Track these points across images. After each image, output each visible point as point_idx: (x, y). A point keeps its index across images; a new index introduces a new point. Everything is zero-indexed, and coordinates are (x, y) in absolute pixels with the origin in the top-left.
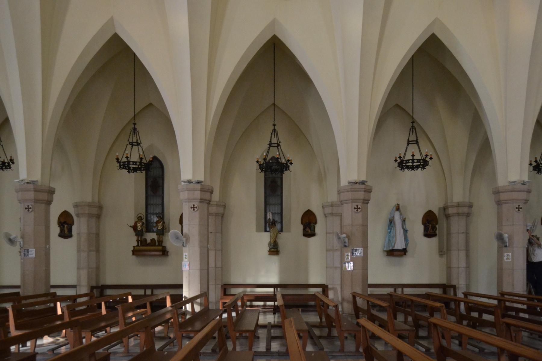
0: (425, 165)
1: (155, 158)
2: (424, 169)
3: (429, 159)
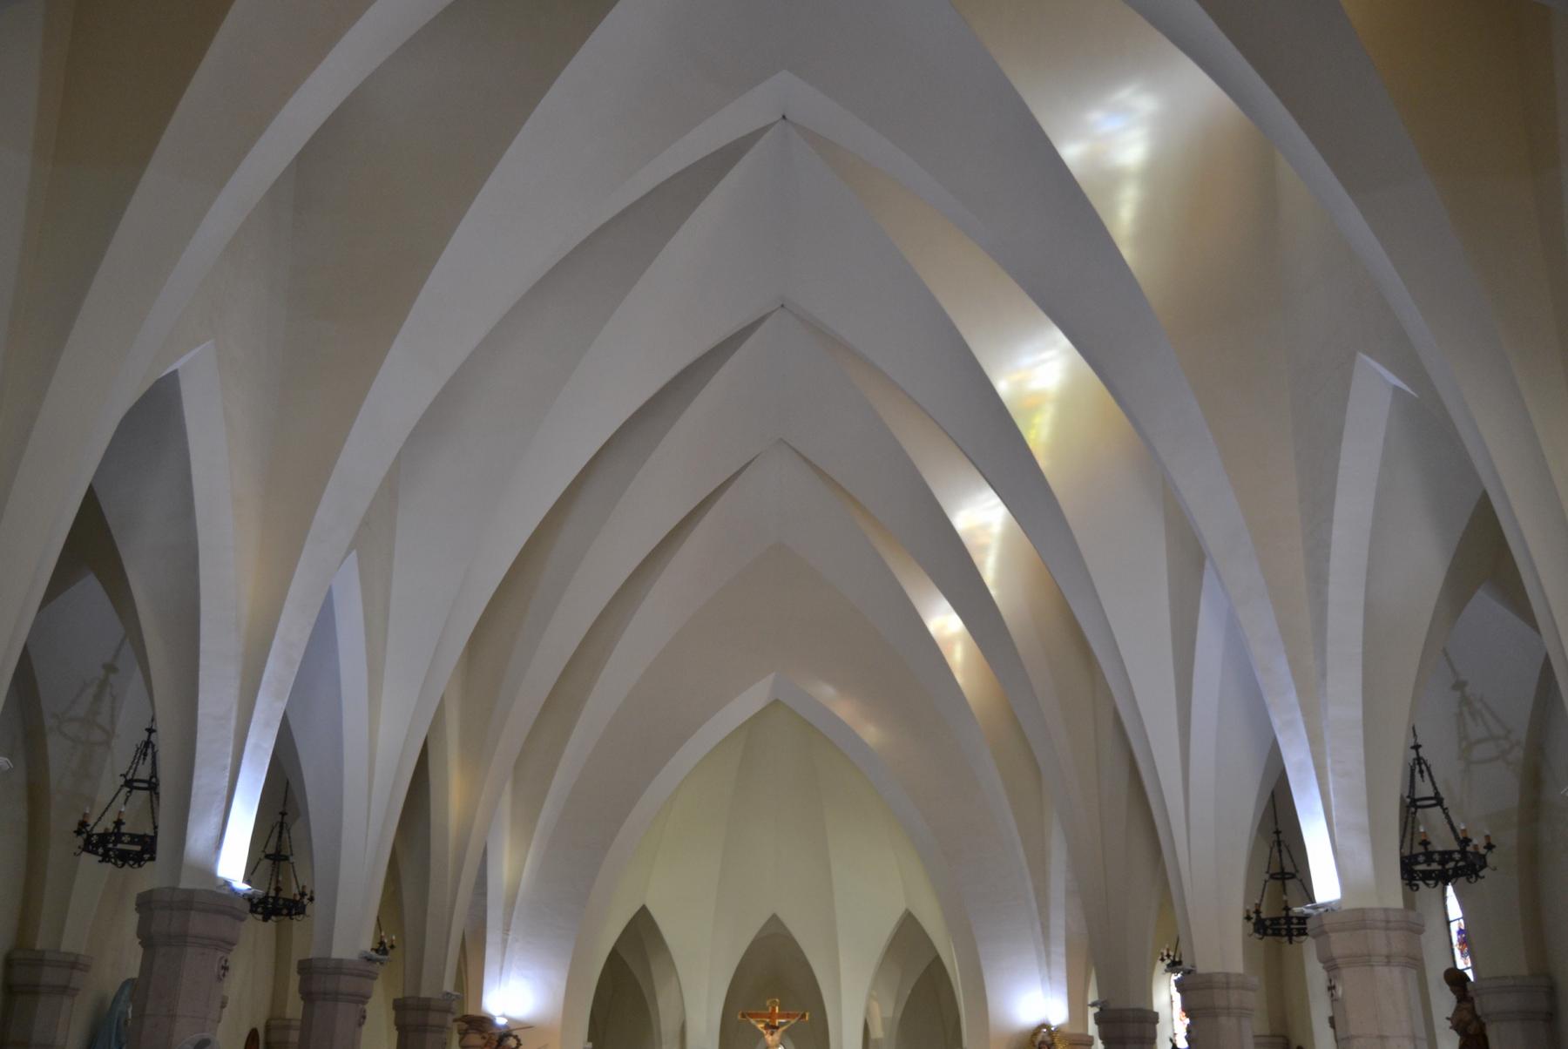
0: (1477, 866)
1: (78, 990)
2: (1479, 880)
3: (1485, 847)
